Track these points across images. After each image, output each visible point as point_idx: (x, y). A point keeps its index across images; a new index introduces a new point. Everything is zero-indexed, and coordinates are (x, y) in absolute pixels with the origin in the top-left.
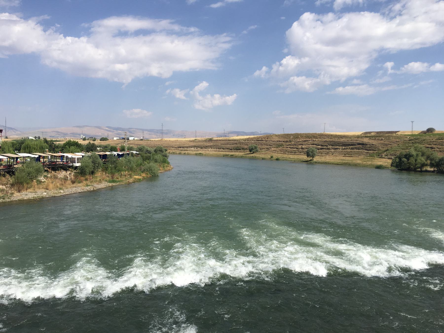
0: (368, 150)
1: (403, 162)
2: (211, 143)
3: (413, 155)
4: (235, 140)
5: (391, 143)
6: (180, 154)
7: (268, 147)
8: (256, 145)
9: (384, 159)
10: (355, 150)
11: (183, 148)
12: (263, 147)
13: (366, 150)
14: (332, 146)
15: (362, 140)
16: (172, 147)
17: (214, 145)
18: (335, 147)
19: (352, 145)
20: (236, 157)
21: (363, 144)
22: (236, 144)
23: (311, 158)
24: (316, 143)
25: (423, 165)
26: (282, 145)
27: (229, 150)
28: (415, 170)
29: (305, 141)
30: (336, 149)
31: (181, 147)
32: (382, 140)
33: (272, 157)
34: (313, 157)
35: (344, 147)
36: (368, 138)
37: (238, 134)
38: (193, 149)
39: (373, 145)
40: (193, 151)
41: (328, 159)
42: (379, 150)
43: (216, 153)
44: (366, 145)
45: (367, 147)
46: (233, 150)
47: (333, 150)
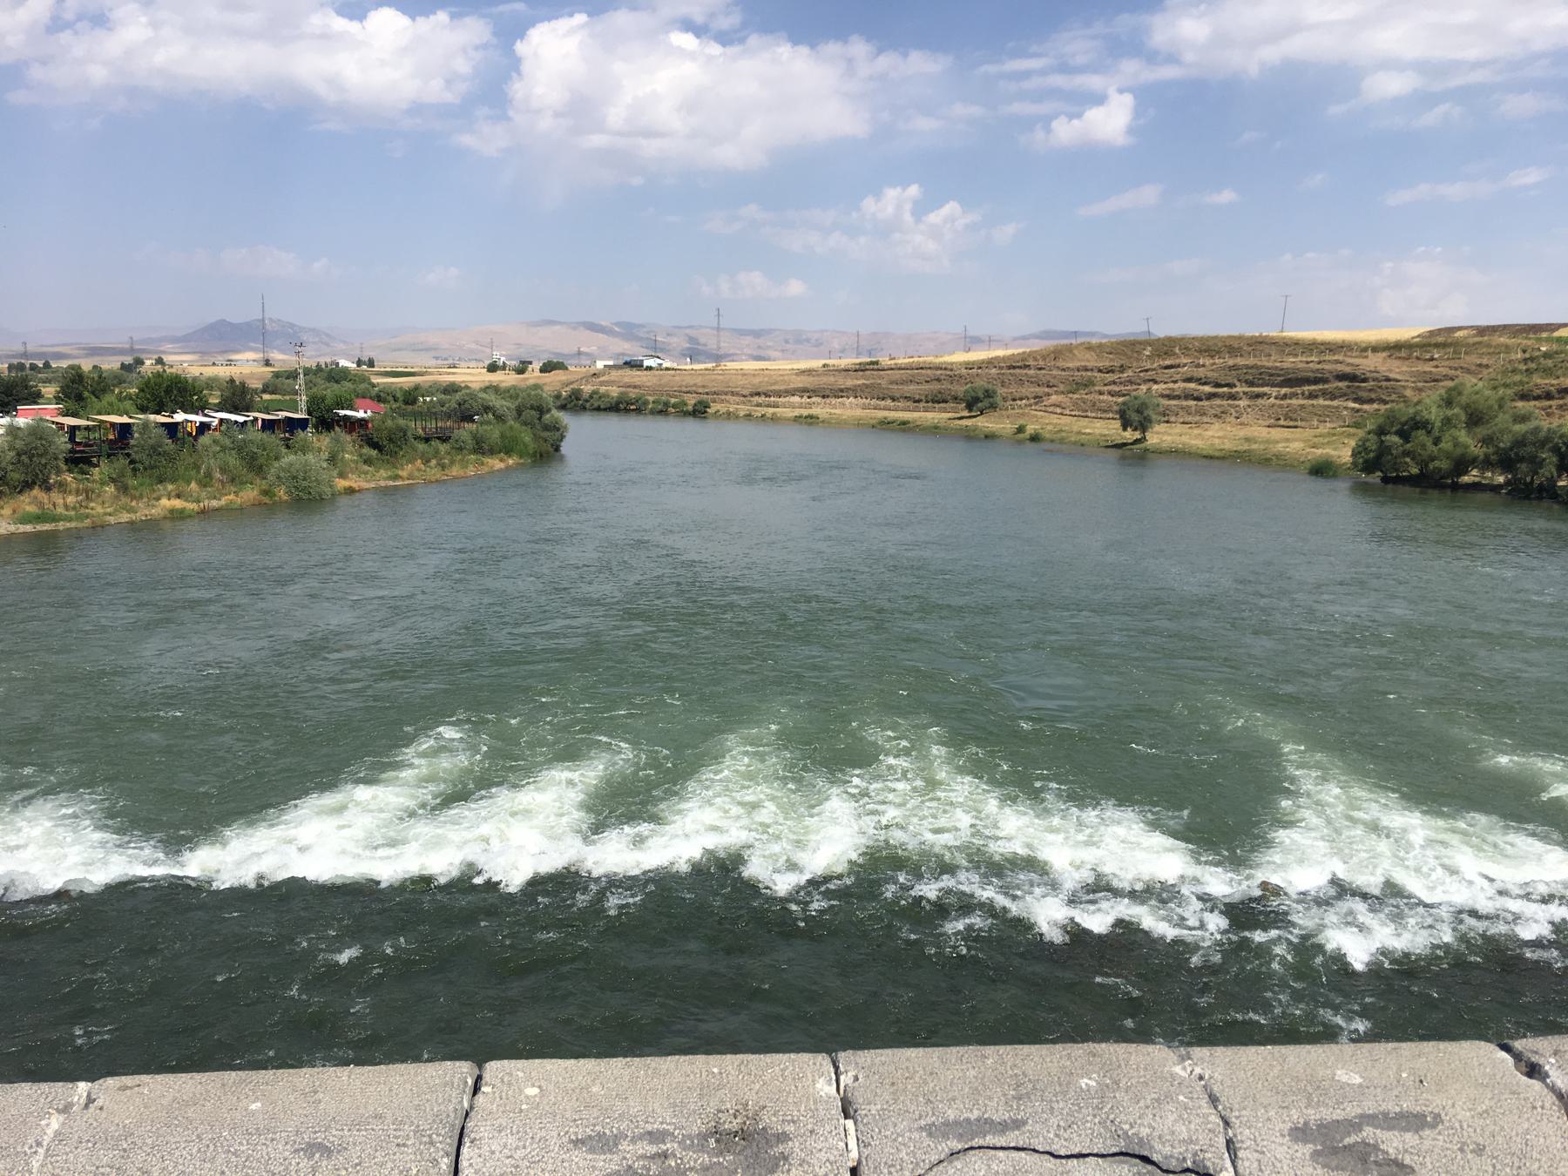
2: (871, 381)
3: (1427, 422)
6: (749, 416)
7: (1041, 390)
10: (1321, 402)
11: (767, 395)
12: (1024, 391)
13: (1356, 400)
14: (1251, 384)
16: (733, 394)
17: (867, 386)
21: (1352, 378)
22: (938, 380)
23: (1137, 435)
24: (1201, 373)
26: (1089, 384)
29: (1167, 367)
30: (1258, 396)
31: (758, 394)
33: (1021, 430)
35: (1284, 391)
36: (1385, 354)
37: (971, 342)
38: (796, 399)
39: (1388, 380)
40: (793, 407)
41: (1215, 435)
44: (1365, 380)
45: (1365, 389)
46: (922, 405)
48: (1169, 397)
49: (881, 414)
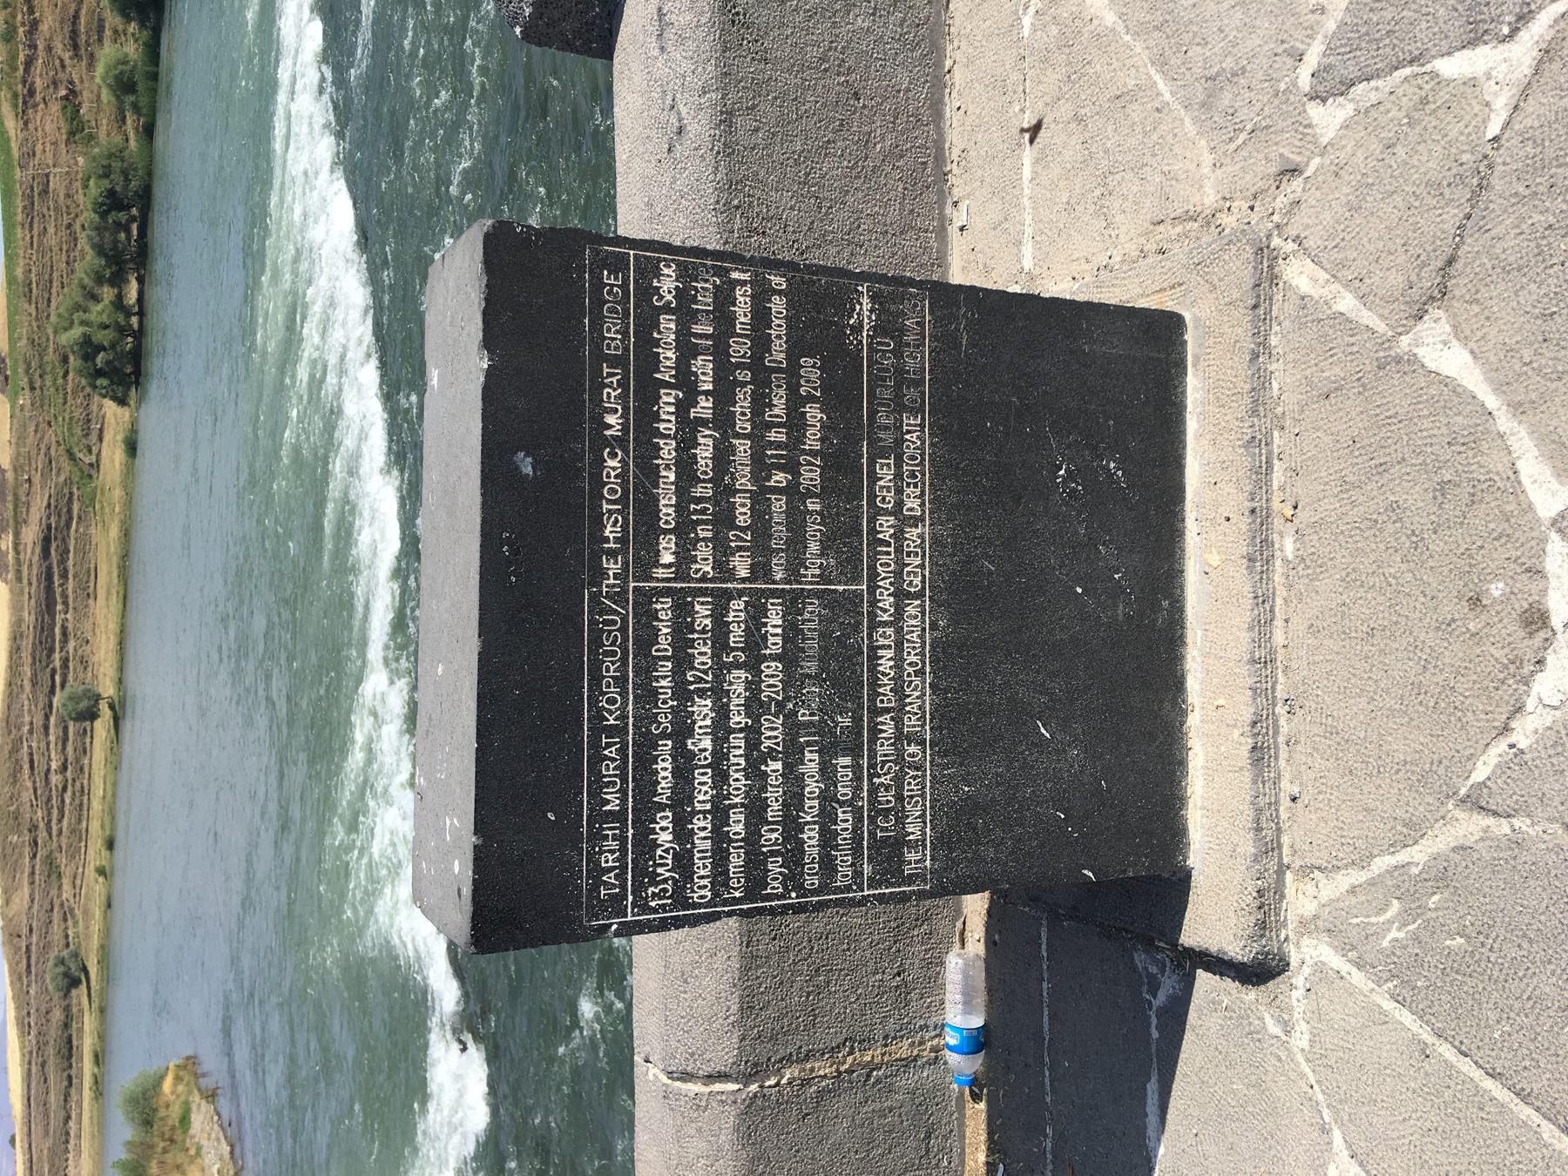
0: (71, 518)
1: (108, 363)
3: (84, 334)
4: (28, 1076)
5: (43, 447)
8: (51, 963)
9: (104, 453)
10: (70, 563)
14: (51, 650)
15: (30, 546)
18: (58, 638)
19: (49, 578)
20: (102, 1036)
21: (46, 541)
22: (43, 1065)
24: (38, 720)
25: (119, 304)
26: (50, 861)
27: (73, 1091)
28: (140, 334)
32: (29, 480)
33: (101, 871)
34: (98, 697)
35: (59, 607)
39: (49, 505)
42: (68, 482)
43: (85, 1144)
44: (49, 527)
46: (73, 1072)
47: (71, 645)
48: (65, 740)
49: (87, 1094)
